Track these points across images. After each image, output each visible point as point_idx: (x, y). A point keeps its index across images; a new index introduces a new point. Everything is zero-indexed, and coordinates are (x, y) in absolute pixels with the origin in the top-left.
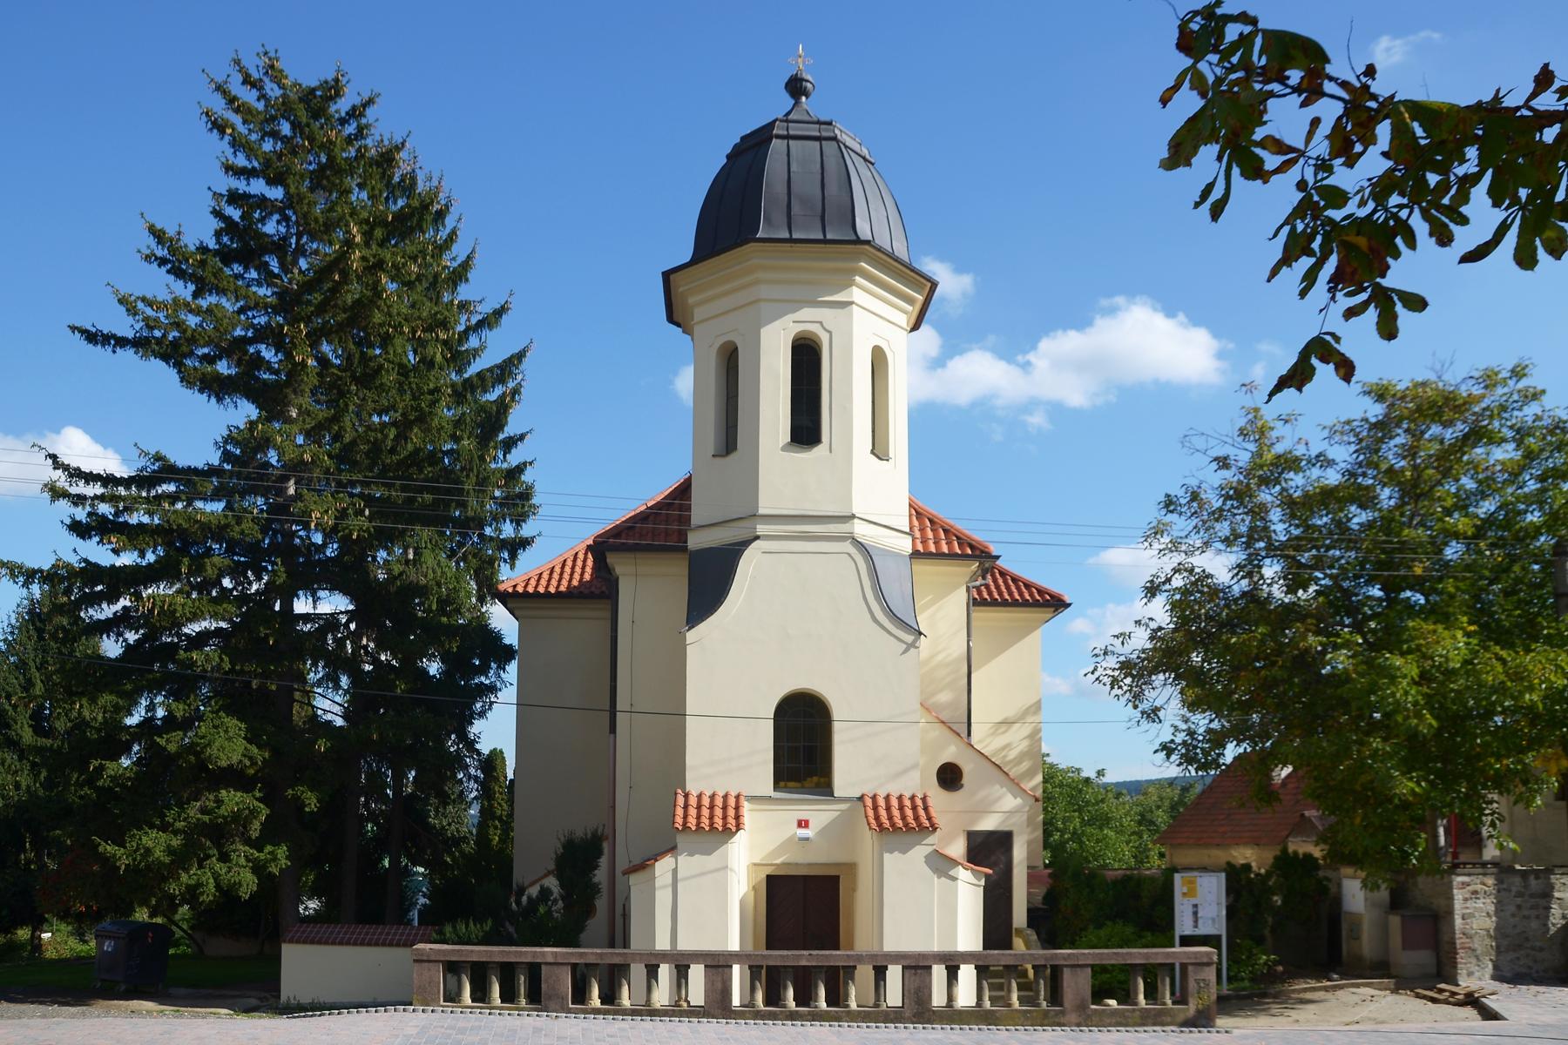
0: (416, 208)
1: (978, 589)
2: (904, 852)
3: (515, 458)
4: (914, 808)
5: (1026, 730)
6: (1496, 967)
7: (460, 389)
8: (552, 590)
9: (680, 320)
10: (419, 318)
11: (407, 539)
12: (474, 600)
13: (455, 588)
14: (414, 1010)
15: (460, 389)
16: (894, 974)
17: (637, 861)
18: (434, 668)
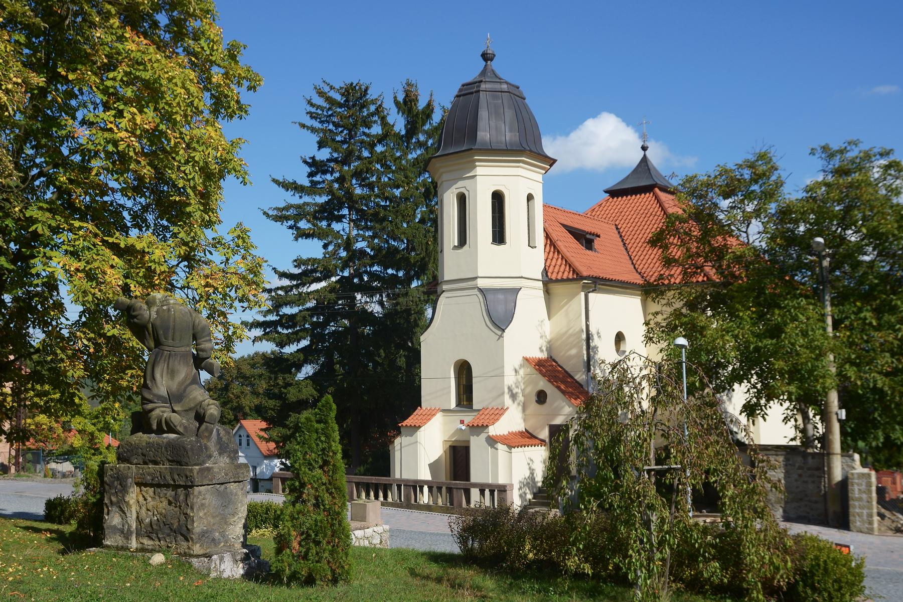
2: (478, 436)
6: (784, 511)
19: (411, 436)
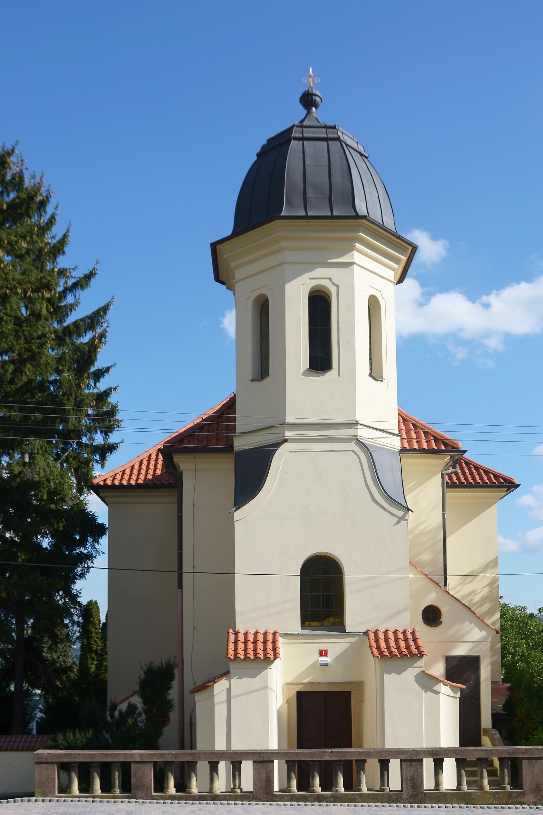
0: (24, 199)
1: (449, 475)
2: (399, 673)
3: (103, 385)
4: (406, 640)
5: (487, 580)
7: (61, 335)
8: (133, 482)
9: (225, 280)
10: (29, 282)
11: (24, 447)
12: (74, 491)
13: (60, 483)
14: (36, 801)
15: (61, 335)
16: (395, 765)
17: (200, 683)
18: (46, 543)
19: (254, 676)
